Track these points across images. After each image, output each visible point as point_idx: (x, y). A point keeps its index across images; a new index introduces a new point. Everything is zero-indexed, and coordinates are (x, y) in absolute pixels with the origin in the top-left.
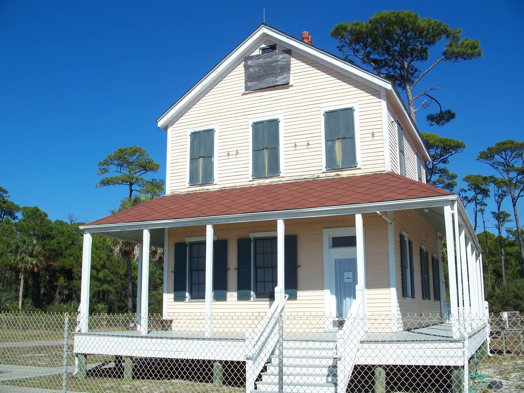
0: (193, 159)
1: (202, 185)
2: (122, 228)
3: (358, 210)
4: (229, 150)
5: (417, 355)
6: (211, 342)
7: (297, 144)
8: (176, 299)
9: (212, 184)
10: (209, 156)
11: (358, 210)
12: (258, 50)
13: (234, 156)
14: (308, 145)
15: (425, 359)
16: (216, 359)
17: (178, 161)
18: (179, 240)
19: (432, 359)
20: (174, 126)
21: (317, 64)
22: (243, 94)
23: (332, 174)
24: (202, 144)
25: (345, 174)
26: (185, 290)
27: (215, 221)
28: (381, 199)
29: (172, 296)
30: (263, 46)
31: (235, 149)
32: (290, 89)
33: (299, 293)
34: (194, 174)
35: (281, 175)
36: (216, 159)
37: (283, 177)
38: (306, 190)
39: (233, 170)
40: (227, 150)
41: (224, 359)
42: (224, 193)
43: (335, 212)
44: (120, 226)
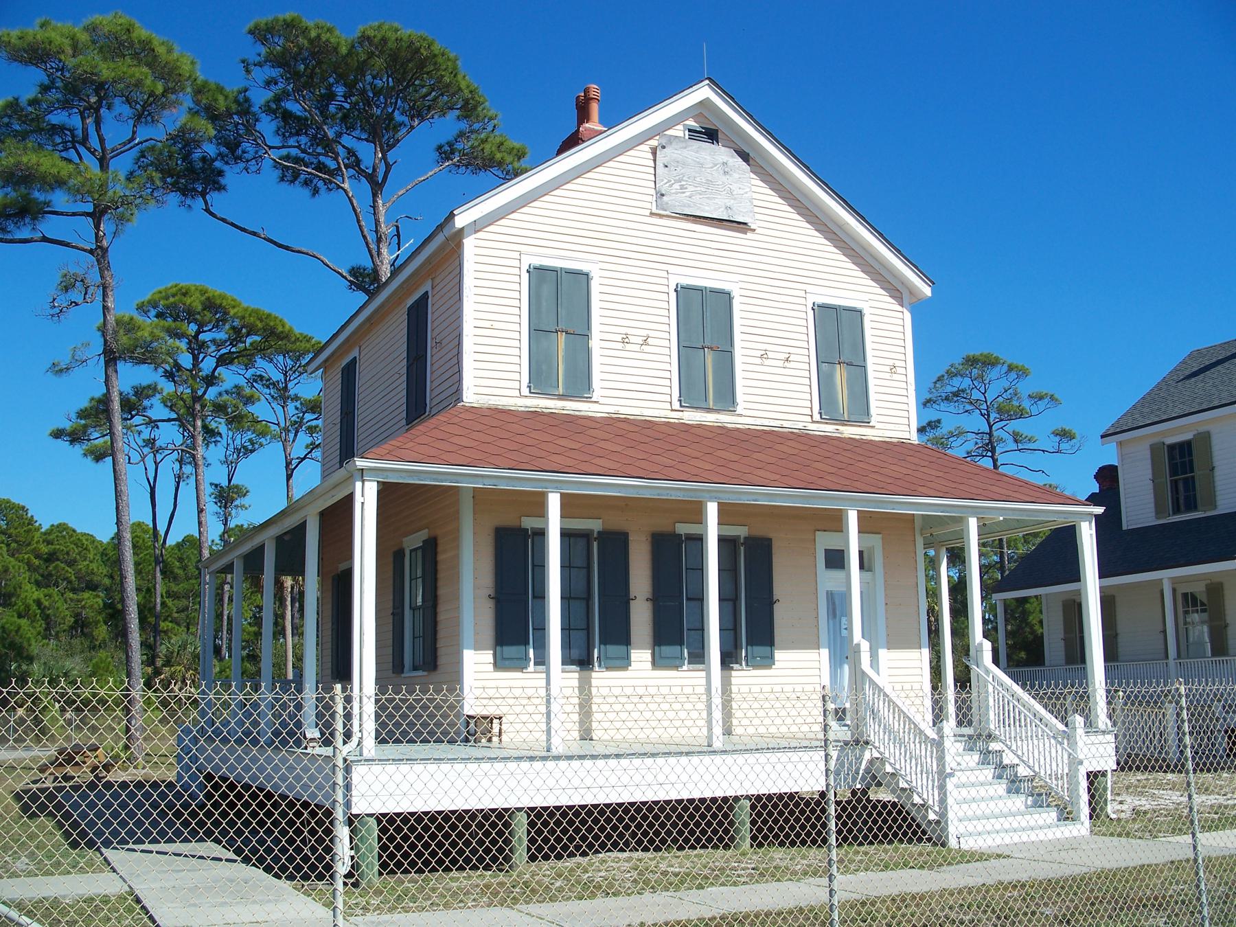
0: (536, 331)
1: (562, 397)
2: (487, 481)
3: (974, 511)
4: (651, 334)
5: (370, 793)
6: (469, 765)
7: (770, 355)
8: (499, 664)
9: (588, 400)
10: (580, 334)
11: (974, 511)
12: (680, 127)
13: (637, 348)
14: (645, 343)
15: (582, 791)
16: (739, 794)
17: (496, 325)
18: (508, 520)
19: (570, 792)
20: (479, 235)
21: (798, 204)
22: (652, 214)
23: (829, 429)
24: (559, 301)
25: (849, 431)
26: (526, 643)
27: (721, 495)
28: (513, 464)
29: (488, 656)
30: (691, 123)
31: (645, 333)
32: (750, 235)
33: (779, 655)
34: (544, 367)
35: (739, 410)
36: (595, 343)
37: (740, 415)
38: (632, 439)
39: (633, 378)
40: (624, 330)
41: (753, 791)
42: (618, 427)
43: (471, 479)
44: (482, 476)
